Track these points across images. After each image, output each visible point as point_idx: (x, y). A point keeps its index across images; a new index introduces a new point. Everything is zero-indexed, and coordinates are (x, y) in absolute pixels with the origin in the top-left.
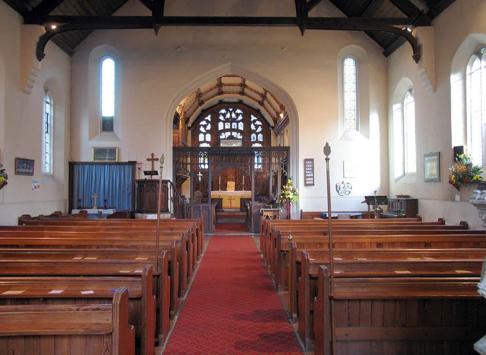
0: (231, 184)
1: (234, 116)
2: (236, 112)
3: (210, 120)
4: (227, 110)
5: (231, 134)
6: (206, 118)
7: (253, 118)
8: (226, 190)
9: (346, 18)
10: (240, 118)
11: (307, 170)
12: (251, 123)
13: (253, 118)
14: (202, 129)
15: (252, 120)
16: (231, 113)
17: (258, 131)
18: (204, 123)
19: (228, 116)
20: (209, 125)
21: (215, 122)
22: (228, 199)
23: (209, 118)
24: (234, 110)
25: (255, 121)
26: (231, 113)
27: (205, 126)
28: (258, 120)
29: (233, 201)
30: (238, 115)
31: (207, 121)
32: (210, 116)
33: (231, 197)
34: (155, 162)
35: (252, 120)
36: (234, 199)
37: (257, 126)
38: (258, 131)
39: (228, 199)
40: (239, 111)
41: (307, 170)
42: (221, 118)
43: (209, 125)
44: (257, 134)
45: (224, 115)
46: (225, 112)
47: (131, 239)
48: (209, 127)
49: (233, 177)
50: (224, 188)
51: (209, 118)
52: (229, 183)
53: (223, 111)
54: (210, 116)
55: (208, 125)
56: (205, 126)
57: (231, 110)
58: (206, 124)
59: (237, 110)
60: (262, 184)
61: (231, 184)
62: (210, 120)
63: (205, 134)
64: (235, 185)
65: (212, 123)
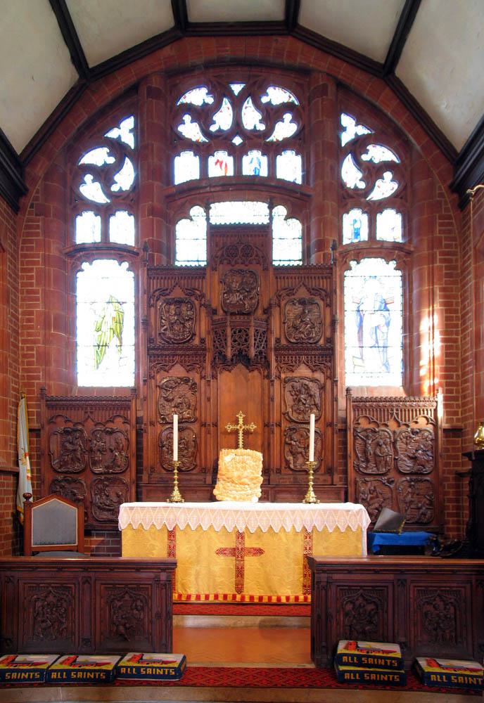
0: (241, 466)
1: (252, 118)
2: (264, 100)
3: (129, 140)
4: (220, 91)
5: (272, 166)
6: (113, 134)
7: (351, 129)
8: (213, 499)
9: (368, 134)
10: (286, 129)
11: (288, 357)
12: (338, 153)
13: (351, 129)
14: (91, 190)
15: (346, 138)
16: (237, 104)
17: (376, 195)
18: (98, 156)
19: (223, 120)
20: (128, 166)
21: (158, 146)
22: (221, 552)
23: (125, 131)
24: (254, 92)
25: (358, 146)
26: (237, 104)
27: (105, 175)
28: (378, 138)
29: (250, 562)
30: (271, 115)
31: (118, 149)
32: (129, 123)
33: (240, 536)
34: (373, 343)
35: (346, 138)
36: (259, 552)
37: (372, 172)
38: (376, 195)
39: (221, 552)
40: (277, 96)
41: (288, 357)
42: (190, 129)
43: (128, 166)
44: (372, 210)
45: (203, 115)
46: (210, 100)
47: (197, 333)
48: (126, 178)
49: (252, 427)
50: (201, 483)
51: (125, 131)
52: (228, 459)
53: (198, 96)
54: (129, 123)
55: (118, 166)
56: (105, 175)
57: (237, 88)
58: (111, 160)
59: (270, 90)
60: (409, 463)
61: (241, 466)
62: (129, 140)
63: (105, 212)
64: (266, 471)
65: (138, 156)
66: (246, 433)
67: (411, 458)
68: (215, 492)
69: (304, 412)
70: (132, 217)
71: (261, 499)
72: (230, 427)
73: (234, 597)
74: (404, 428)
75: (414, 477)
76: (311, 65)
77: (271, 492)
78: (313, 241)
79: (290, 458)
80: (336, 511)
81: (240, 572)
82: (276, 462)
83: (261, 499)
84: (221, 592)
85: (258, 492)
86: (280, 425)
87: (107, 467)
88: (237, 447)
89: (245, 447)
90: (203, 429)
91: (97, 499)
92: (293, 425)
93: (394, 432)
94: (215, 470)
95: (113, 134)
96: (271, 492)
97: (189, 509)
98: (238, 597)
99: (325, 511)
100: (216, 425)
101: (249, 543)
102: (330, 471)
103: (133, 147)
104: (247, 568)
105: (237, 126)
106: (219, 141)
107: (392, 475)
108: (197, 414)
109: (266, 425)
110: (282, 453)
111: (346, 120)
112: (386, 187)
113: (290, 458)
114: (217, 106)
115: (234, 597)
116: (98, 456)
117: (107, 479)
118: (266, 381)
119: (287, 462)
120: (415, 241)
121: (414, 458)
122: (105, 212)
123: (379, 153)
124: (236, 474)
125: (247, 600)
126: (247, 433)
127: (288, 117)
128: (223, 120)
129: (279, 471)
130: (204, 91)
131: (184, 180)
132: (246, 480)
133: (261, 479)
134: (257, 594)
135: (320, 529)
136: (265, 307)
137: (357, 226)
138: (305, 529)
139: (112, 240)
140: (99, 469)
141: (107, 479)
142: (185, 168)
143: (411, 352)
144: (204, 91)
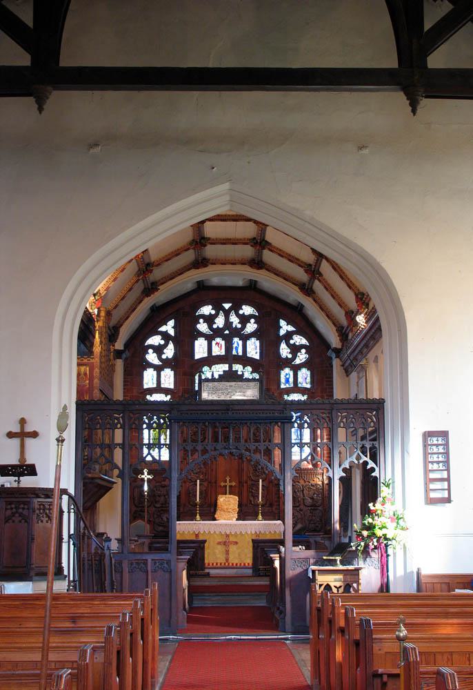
0: (228, 503)
4: (218, 308)
6: (163, 329)
7: (285, 327)
8: (215, 519)
10: (251, 327)
12: (279, 340)
13: (285, 327)
14: (152, 357)
15: (282, 332)
17: (298, 361)
18: (156, 340)
19: (220, 322)
20: (171, 346)
21: (185, 338)
22: (219, 543)
23: (169, 327)
24: (236, 308)
25: (289, 336)
27: (159, 350)
29: (233, 548)
30: (244, 320)
31: (165, 336)
33: (227, 536)
35: (282, 332)
36: (236, 543)
37: (295, 349)
38: (298, 361)
39: (219, 543)
40: (247, 310)
42: (203, 327)
45: (210, 320)
46: (213, 312)
48: (169, 352)
49: (234, 484)
50: (210, 512)
51: (169, 327)
53: (207, 310)
54: (171, 323)
55: (166, 345)
57: (227, 306)
60: (310, 500)
61: (228, 503)
63: (159, 369)
64: (240, 505)
65: (176, 340)
66: (231, 486)
67: (311, 498)
68: (216, 516)
69: (258, 476)
70: (173, 372)
71: (237, 520)
72: (222, 484)
73: (225, 564)
74: (307, 483)
75: (313, 508)
76: (310, 668)
77: (242, 516)
78: (264, 387)
79: (252, 499)
80: (270, 524)
81: (227, 552)
82: (245, 501)
83: (237, 520)
84: (219, 562)
85: (236, 515)
86: (246, 482)
87: (162, 504)
88: (226, 494)
89: (230, 494)
90: (210, 485)
91: (157, 521)
92: (253, 482)
93: (303, 486)
94: (216, 505)
95: (163, 329)
96: (242, 516)
97: (205, 524)
98: (227, 564)
99: (265, 524)
100: (216, 483)
101: (232, 539)
102: (271, 505)
103: (173, 335)
104: (231, 550)
105: (228, 324)
106: (218, 333)
107: (302, 507)
108: (207, 477)
109: (240, 482)
110: (248, 497)
111: (283, 323)
112: (302, 357)
113: (252, 499)
114: (216, 315)
115: (225, 564)
116: (158, 499)
117: (162, 510)
118: (240, 461)
119: (251, 501)
120: (315, 387)
121: (312, 498)
122: (159, 369)
123: (298, 340)
124: (225, 507)
125: (231, 564)
126: (231, 486)
127: (252, 321)
128: (220, 322)
129: (246, 505)
130: (210, 307)
131: (199, 357)
132: (230, 510)
133: (238, 509)
134: (235, 562)
135: (263, 532)
136: (245, 438)
137: (287, 377)
138: (256, 532)
139: (162, 386)
140: (158, 505)
141: (162, 510)
142: (200, 349)
143: (314, 436)
144: (210, 307)
